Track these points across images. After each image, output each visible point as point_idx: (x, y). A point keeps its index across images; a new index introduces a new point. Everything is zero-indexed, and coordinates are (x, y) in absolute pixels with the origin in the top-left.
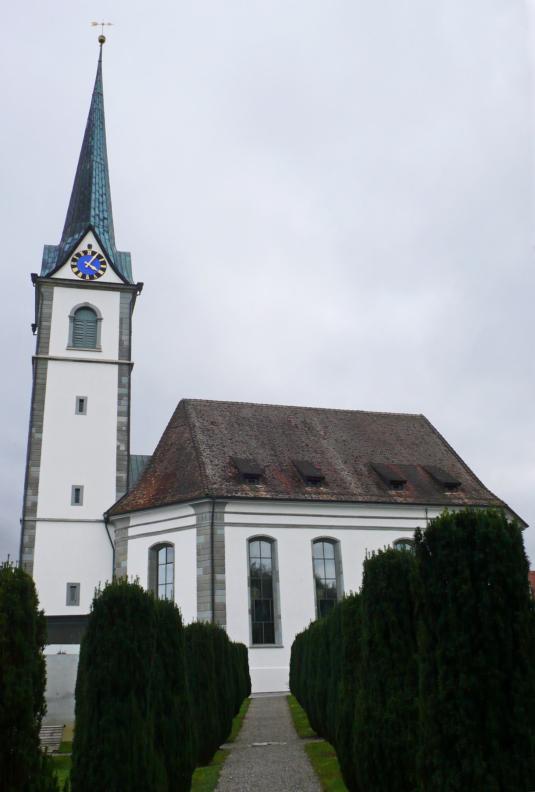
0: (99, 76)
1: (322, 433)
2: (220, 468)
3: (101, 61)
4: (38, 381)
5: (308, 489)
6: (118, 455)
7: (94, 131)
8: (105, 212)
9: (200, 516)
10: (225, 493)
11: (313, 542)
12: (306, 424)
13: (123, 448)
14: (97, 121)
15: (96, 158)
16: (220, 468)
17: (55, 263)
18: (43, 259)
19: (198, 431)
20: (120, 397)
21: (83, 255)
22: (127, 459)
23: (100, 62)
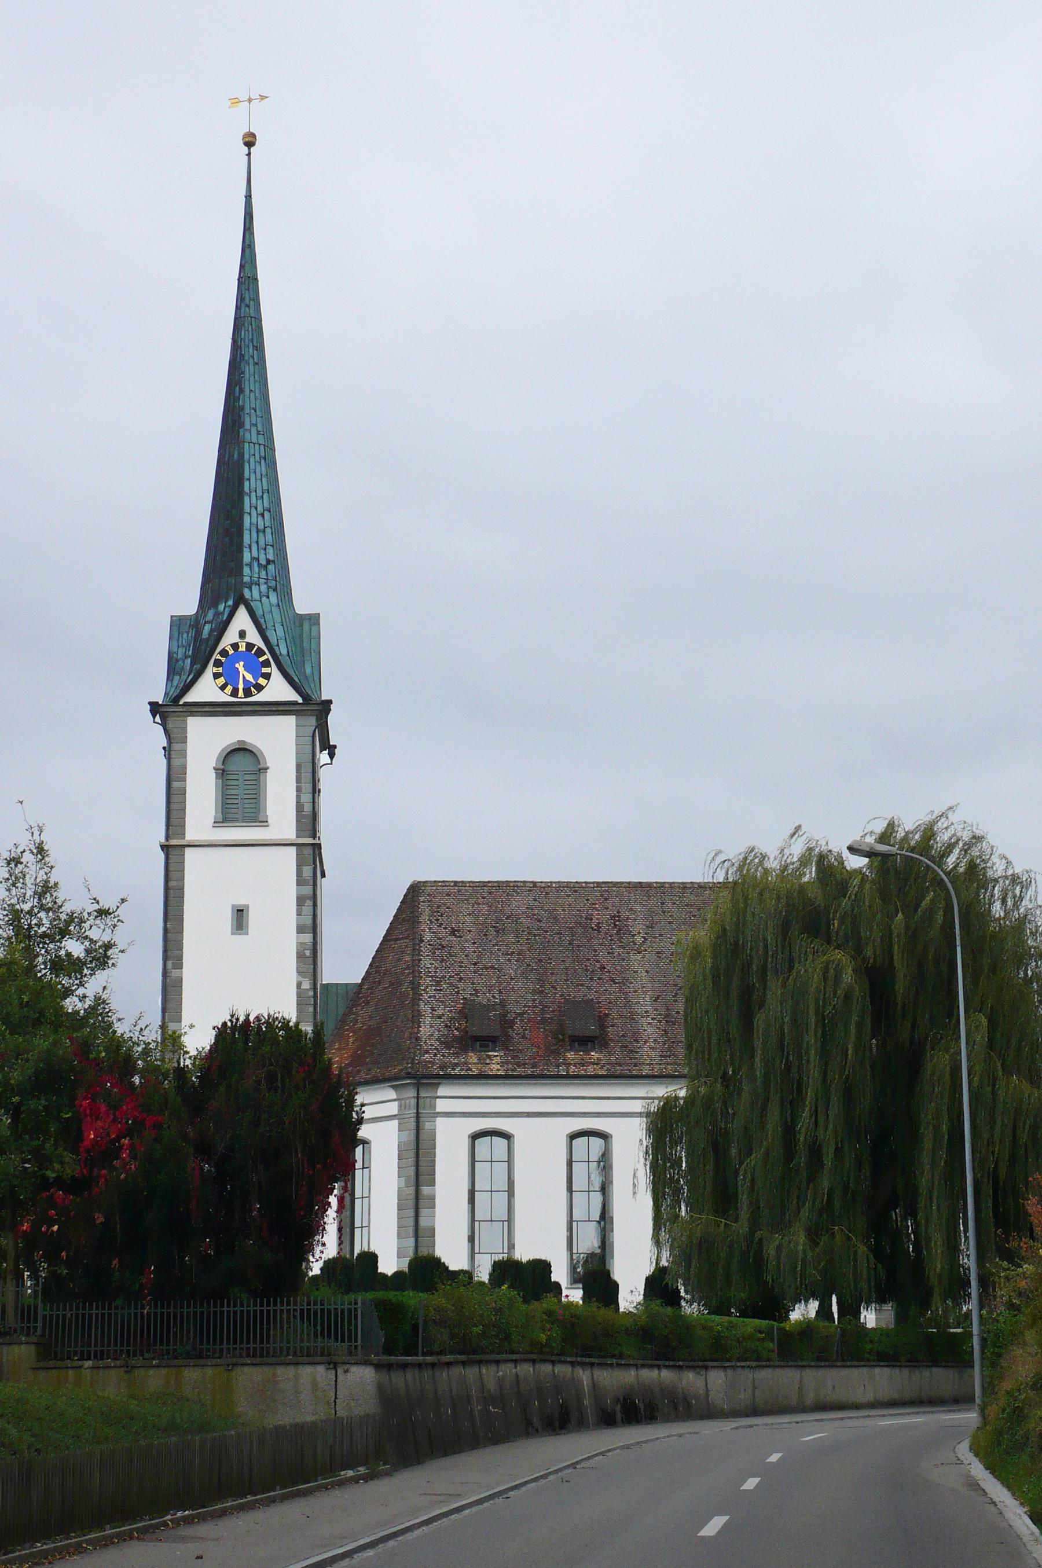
0: (247, 251)
1: (639, 939)
2: (442, 1022)
3: (250, 196)
4: (172, 884)
5: (570, 1055)
6: (299, 995)
7: (243, 373)
8: (270, 550)
9: (403, 1102)
10: (436, 1069)
11: (570, 1137)
12: (618, 921)
13: (306, 985)
14: (248, 346)
15: (250, 435)
16: (442, 1022)
17: (189, 659)
18: (169, 653)
19: (425, 949)
20: (300, 901)
21: (231, 652)
22: (312, 1003)
23: (248, 197)
